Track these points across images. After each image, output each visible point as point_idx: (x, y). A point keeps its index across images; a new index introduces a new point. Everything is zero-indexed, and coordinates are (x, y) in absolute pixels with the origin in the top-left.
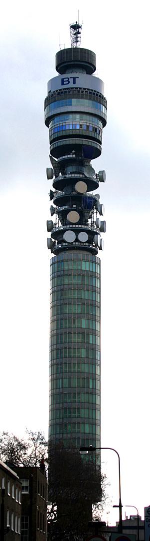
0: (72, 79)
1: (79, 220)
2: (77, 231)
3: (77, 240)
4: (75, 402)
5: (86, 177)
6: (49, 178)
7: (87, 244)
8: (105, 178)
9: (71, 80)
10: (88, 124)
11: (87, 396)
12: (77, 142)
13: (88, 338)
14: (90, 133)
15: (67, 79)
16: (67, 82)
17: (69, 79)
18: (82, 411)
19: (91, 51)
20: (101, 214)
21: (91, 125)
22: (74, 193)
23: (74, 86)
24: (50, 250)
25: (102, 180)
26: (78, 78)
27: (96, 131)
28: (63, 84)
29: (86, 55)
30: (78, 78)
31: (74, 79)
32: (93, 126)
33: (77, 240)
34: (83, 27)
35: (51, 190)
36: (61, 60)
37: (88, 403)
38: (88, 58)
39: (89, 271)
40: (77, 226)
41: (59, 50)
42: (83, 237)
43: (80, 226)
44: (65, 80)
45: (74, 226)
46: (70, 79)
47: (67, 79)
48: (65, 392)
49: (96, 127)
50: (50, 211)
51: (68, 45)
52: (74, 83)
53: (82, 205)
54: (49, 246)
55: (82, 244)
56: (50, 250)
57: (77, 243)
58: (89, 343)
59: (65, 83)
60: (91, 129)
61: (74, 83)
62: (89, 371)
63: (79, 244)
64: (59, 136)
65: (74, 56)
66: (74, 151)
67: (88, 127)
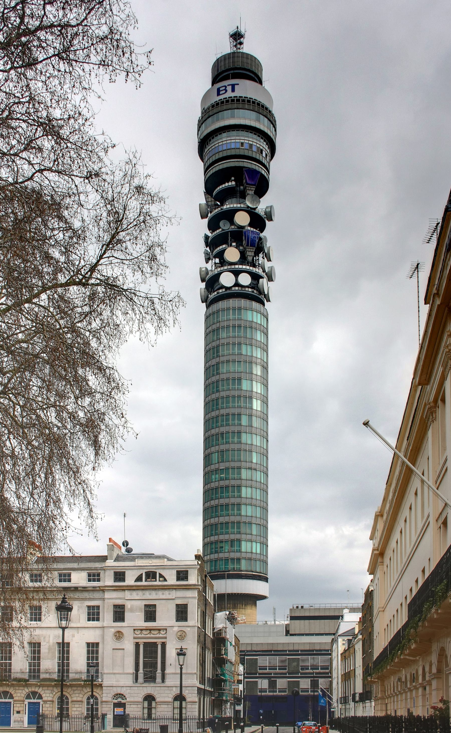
0: (231, 86)
1: (240, 258)
2: (236, 273)
3: (237, 284)
4: (235, 479)
5: (248, 207)
6: (203, 217)
7: (250, 290)
8: (274, 216)
9: (229, 88)
10: (251, 143)
11: (249, 472)
12: (237, 164)
13: (251, 403)
14: (254, 153)
15: (224, 88)
16: (224, 91)
17: (226, 87)
18: (244, 489)
19: (255, 58)
20: (269, 260)
21: (255, 144)
22: (233, 227)
23: (233, 95)
24: (205, 304)
25: (270, 219)
26: (238, 84)
27: (262, 153)
28: (218, 94)
29: (249, 61)
30: (238, 84)
31: (233, 86)
32: (258, 145)
33: (237, 284)
34: (246, 36)
35: (205, 234)
36: (218, 70)
37: (252, 480)
38: (251, 65)
39: (252, 321)
40: (237, 266)
41: (215, 59)
42: (245, 280)
43: (240, 267)
44: (221, 89)
45: (233, 267)
46: (227, 87)
47: (224, 88)
48: (223, 468)
49: (262, 148)
50: (204, 255)
51: (196, 554)
52: (233, 90)
53: (244, 242)
54: (203, 298)
55: (243, 289)
56: (205, 304)
57: (237, 288)
58: (252, 462)
59: (221, 93)
60: (254, 149)
61: (233, 90)
62: (252, 319)
63: (240, 288)
64: (217, 158)
65: (233, 62)
66: (233, 178)
67: (251, 146)
